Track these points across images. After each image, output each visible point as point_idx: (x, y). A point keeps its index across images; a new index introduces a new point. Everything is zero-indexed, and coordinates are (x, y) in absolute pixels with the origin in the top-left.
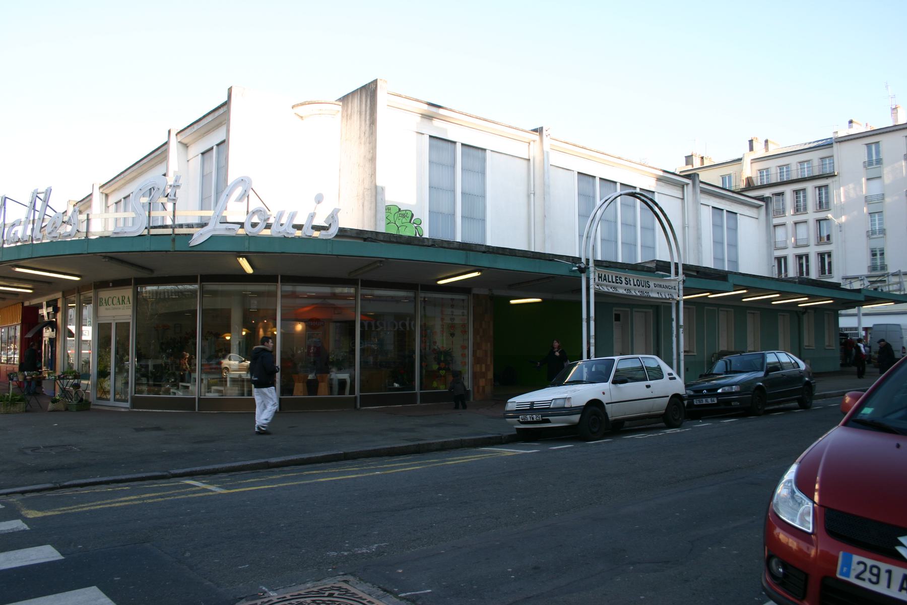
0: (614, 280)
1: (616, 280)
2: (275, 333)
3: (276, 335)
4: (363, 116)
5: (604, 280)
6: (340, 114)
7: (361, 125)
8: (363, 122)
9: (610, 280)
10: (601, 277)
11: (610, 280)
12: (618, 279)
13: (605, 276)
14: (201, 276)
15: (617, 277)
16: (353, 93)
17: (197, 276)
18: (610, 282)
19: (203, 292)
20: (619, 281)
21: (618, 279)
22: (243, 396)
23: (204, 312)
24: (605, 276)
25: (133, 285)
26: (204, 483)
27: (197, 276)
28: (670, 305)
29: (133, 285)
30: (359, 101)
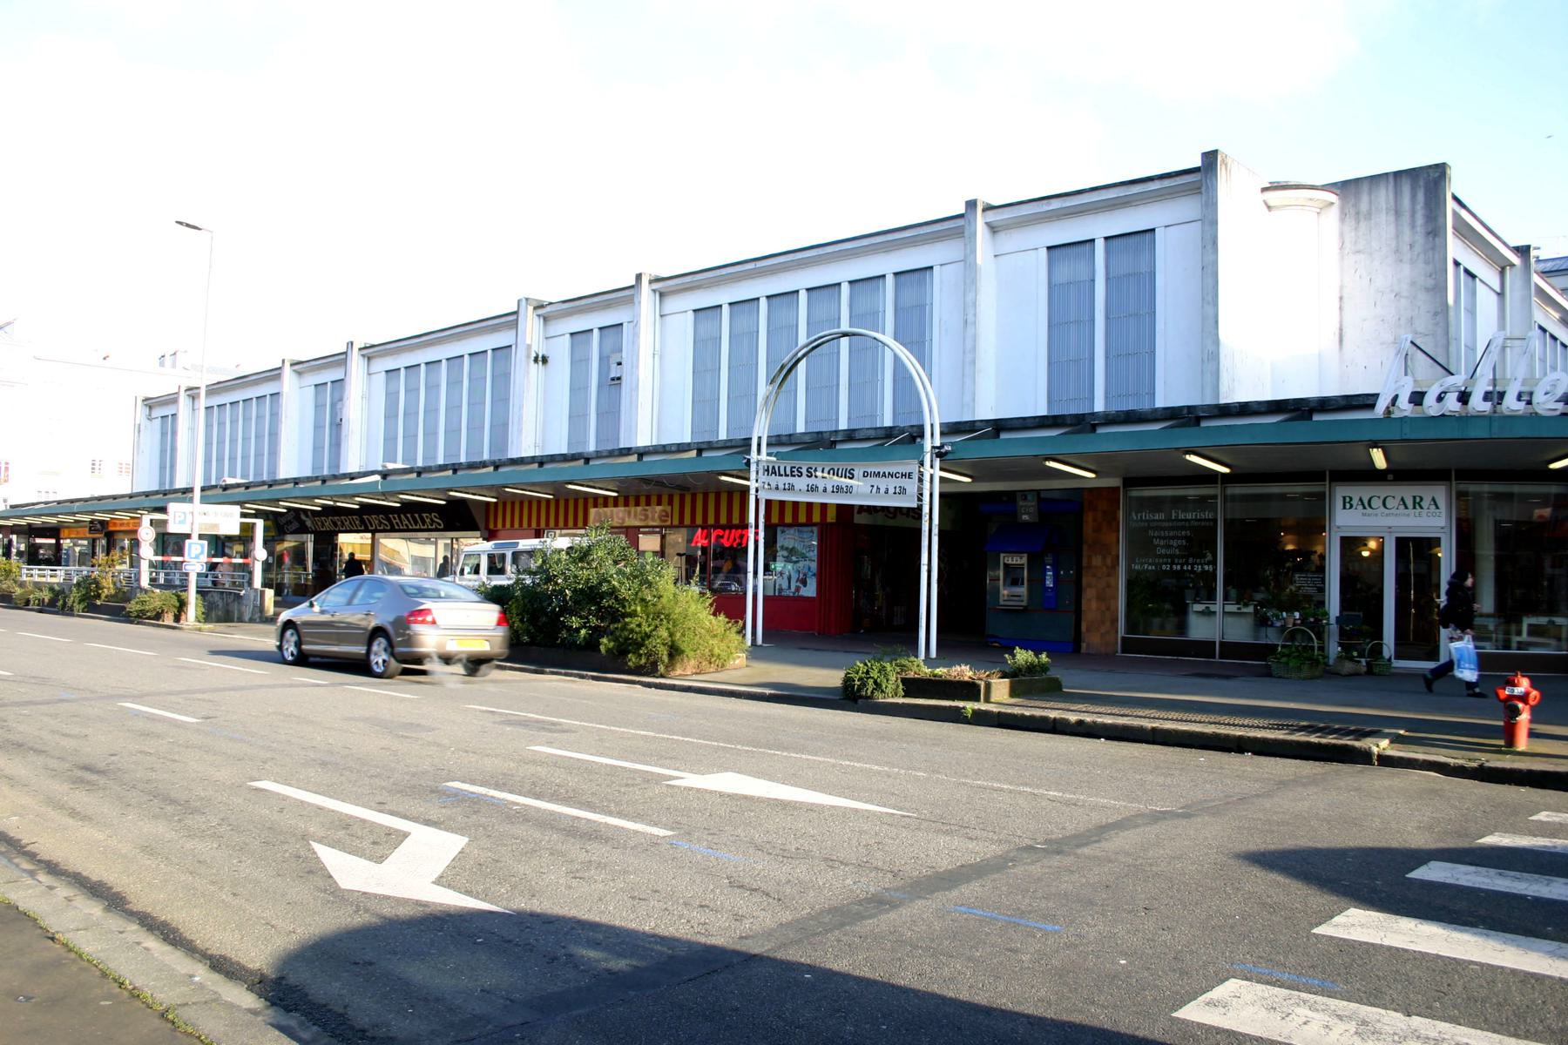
0: (788, 472)
1: (792, 472)
2: (1439, 555)
3: (1439, 558)
4: (1406, 218)
5: (772, 473)
6: (1334, 212)
7: (1398, 236)
8: (1407, 230)
9: (782, 472)
10: (768, 470)
11: (782, 472)
12: (795, 470)
13: (774, 468)
14: (1331, 472)
15: (795, 467)
16: (1374, 180)
17: (1450, 471)
18: (782, 475)
19: (1225, 498)
20: (796, 473)
21: (795, 470)
22: (1509, 648)
23: (1229, 524)
24: (774, 468)
25: (1219, 483)
26: (518, 804)
27: (1325, 472)
28: (908, 523)
29: (1219, 483)
30: (1391, 196)
